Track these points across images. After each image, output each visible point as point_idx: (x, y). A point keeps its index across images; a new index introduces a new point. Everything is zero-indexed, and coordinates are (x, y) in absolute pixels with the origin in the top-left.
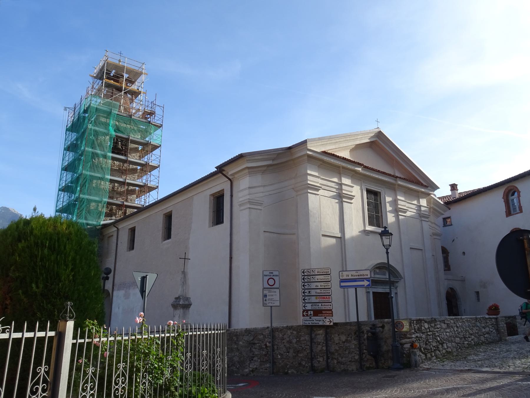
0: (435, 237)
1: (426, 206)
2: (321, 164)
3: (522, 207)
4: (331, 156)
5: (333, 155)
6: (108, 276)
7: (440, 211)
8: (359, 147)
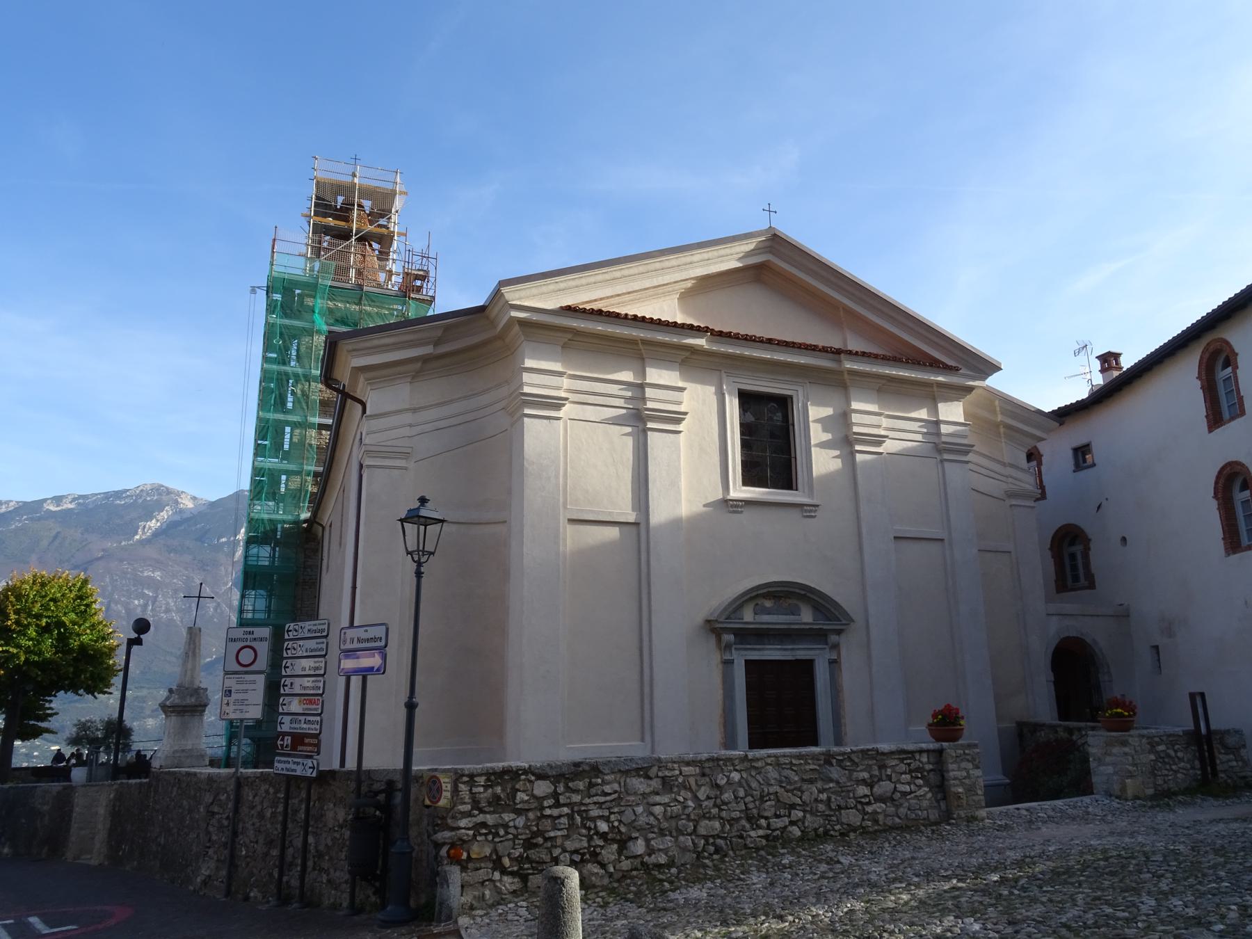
0: (1014, 503)
1: (962, 420)
2: (570, 340)
3: (1244, 399)
4: (593, 317)
5: (611, 315)
6: (136, 635)
7: (1026, 428)
8: (708, 284)
